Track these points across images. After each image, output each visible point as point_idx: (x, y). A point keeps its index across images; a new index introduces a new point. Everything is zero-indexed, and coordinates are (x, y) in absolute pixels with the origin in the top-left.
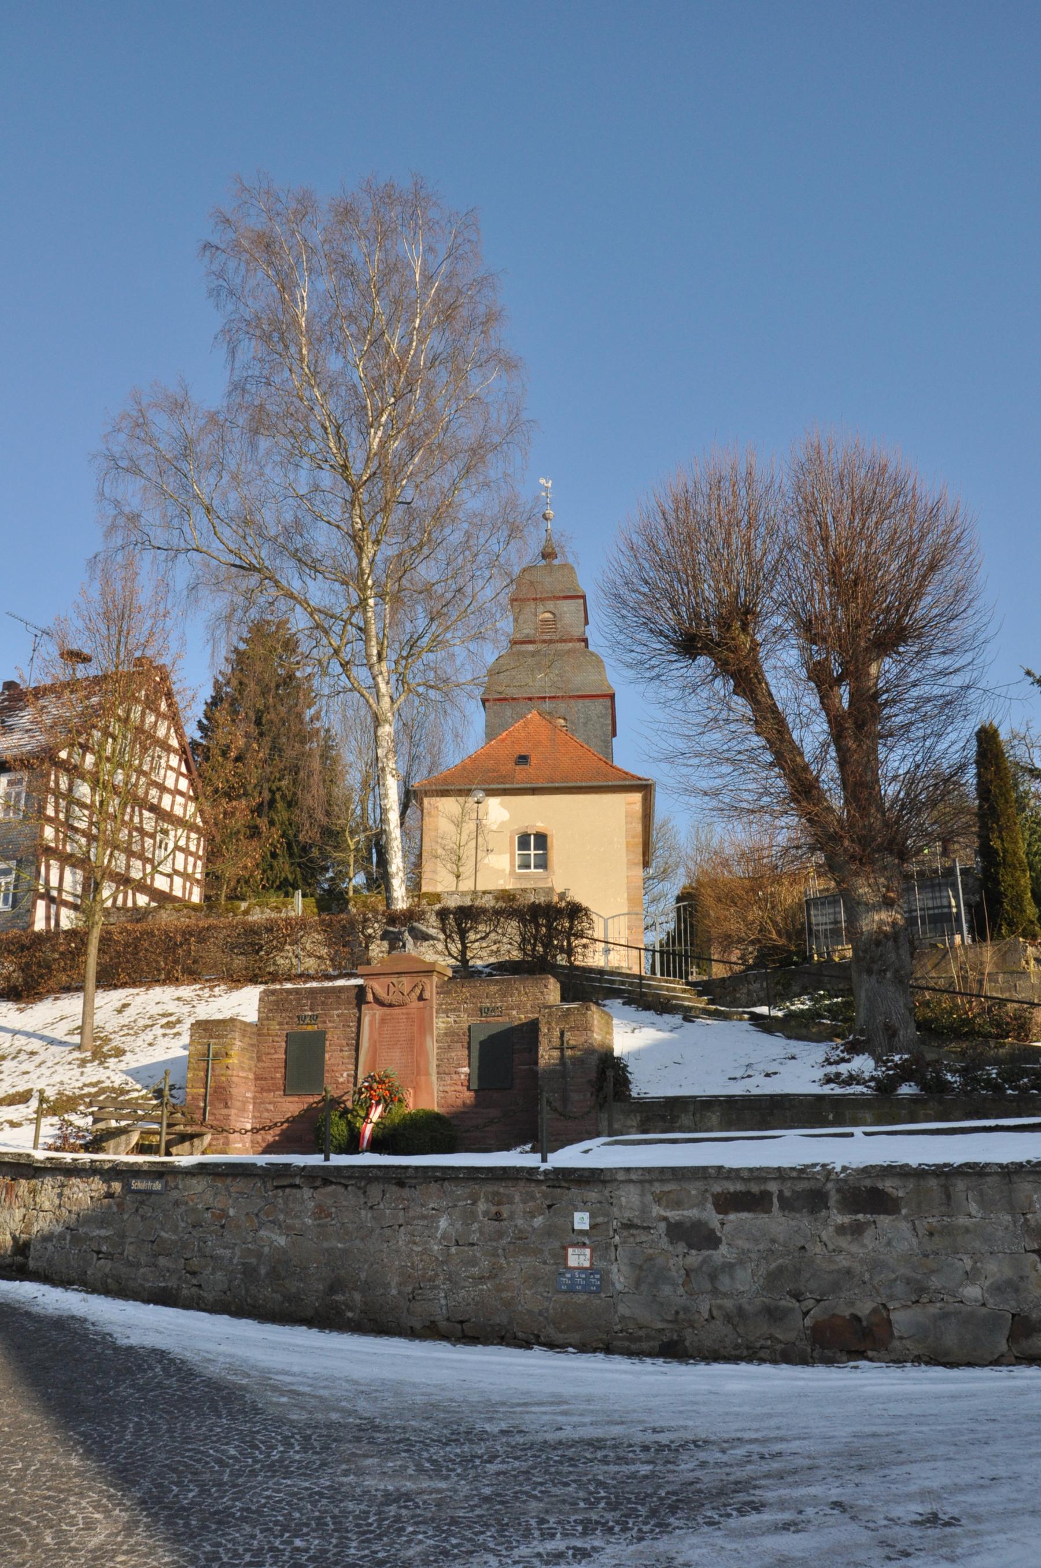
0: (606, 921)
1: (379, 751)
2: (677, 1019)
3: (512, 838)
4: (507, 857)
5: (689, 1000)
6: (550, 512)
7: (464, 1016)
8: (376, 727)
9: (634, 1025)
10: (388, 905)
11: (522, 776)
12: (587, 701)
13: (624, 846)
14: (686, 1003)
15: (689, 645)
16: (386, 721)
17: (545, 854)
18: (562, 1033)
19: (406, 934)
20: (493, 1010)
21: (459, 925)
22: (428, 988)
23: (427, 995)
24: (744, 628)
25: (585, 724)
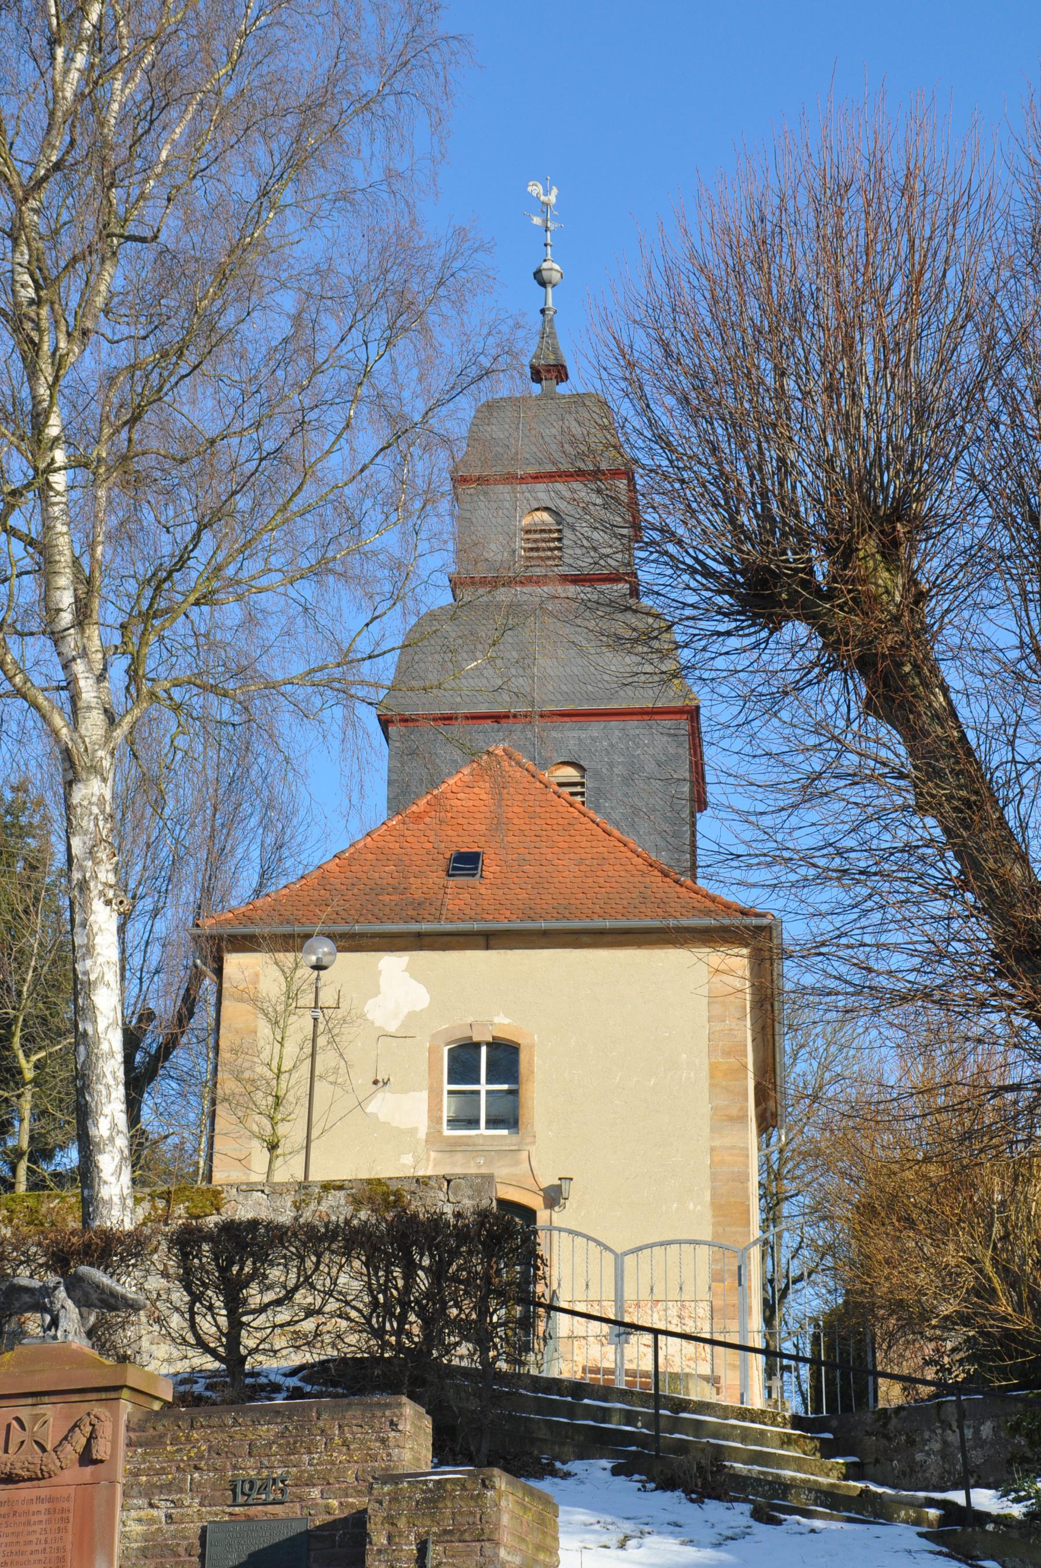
0: (619, 1259)
1: (76, 842)
2: (739, 1515)
3: (433, 1051)
4: (421, 1099)
5: (799, 1465)
6: (553, 268)
7: (192, 1504)
8: (69, 784)
9: (628, 1527)
10: (86, 1218)
11: (462, 902)
12: (633, 725)
13: (705, 1074)
14: (788, 1473)
15: (761, 596)
16: (95, 769)
17: (513, 1093)
18: (422, 1549)
19: (62, 1293)
20: (263, 1489)
21: (224, 1270)
22: (105, 1430)
23: (101, 1450)
24: (890, 550)
25: (628, 780)
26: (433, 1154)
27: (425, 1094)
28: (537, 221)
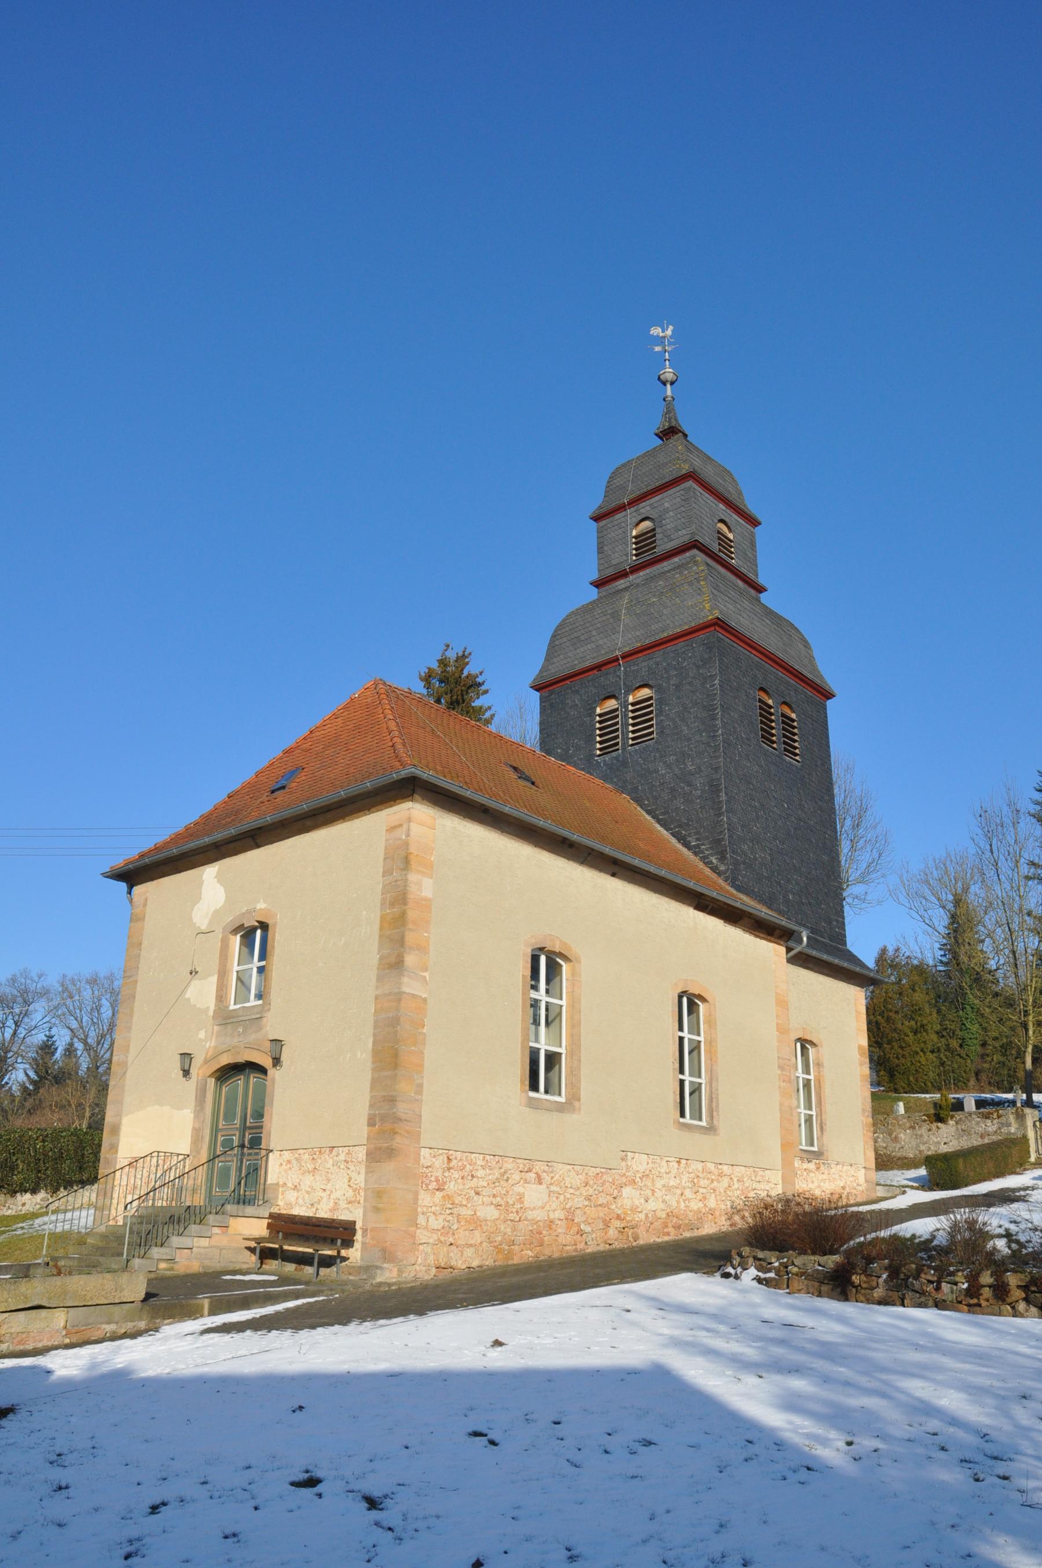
6: (668, 373)
12: (681, 644)
26: (216, 1028)
27: (216, 976)
28: (658, 349)
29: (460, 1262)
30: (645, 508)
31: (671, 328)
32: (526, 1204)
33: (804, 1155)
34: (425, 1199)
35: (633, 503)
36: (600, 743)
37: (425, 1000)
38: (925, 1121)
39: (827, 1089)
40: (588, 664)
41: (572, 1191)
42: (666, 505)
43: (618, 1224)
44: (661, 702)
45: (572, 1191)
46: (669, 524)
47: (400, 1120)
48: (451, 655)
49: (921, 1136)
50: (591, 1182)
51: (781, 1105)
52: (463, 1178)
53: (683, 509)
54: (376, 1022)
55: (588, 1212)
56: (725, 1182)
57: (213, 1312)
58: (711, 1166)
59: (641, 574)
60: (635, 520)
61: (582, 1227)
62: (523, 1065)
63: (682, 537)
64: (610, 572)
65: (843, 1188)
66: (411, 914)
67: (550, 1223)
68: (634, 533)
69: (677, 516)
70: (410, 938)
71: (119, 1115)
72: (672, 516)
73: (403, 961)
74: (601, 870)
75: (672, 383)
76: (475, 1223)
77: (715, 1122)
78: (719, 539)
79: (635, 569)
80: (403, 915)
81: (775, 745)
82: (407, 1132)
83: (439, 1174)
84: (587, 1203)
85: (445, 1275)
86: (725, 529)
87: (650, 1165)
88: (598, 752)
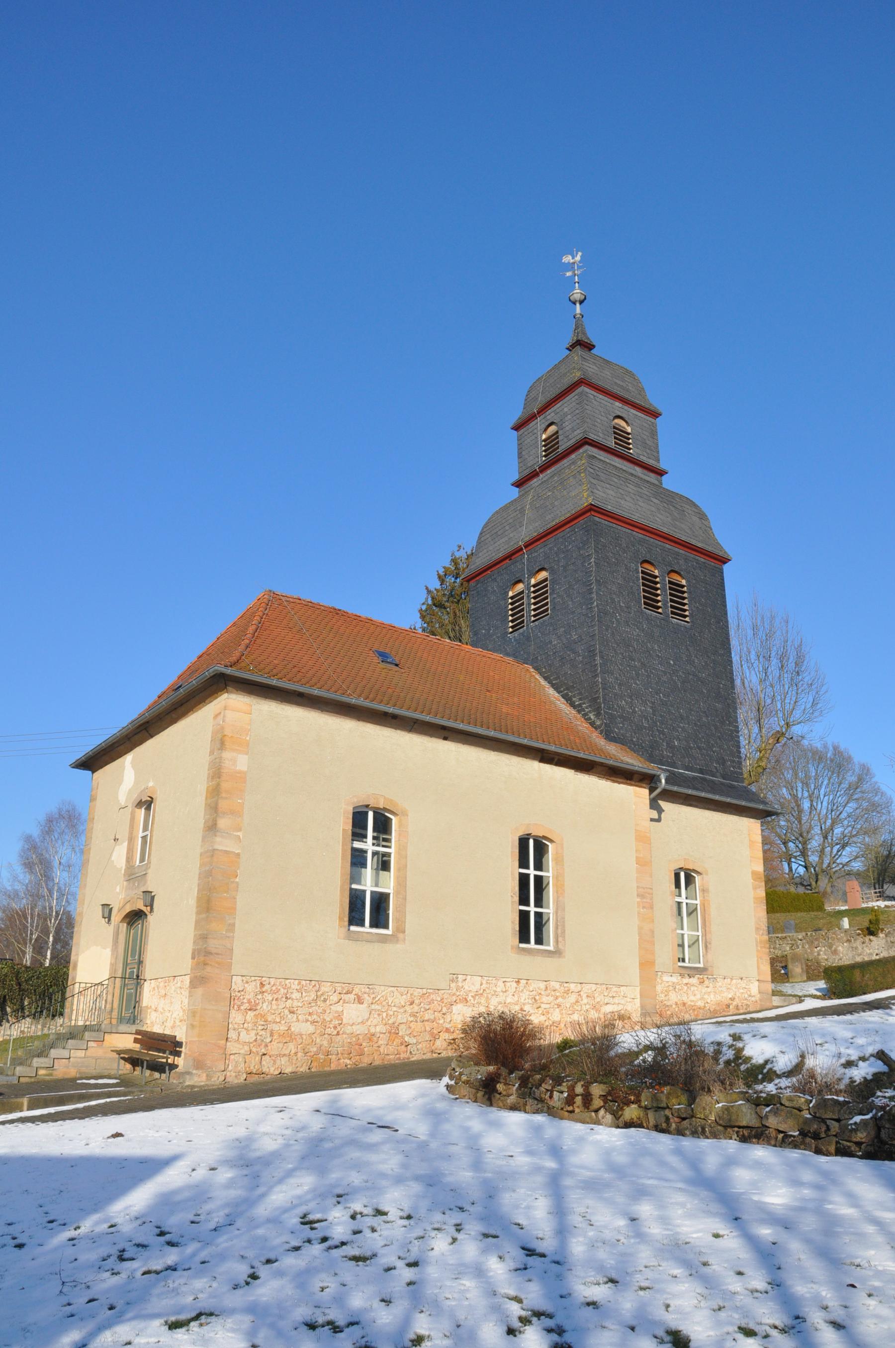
12: (567, 529)
28: (569, 274)
29: (272, 1069)
30: (550, 415)
31: (580, 254)
32: (345, 1021)
33: (683, 971)
34: (236, 1017)
35: (542, 410)
36: (512, 621)
37: (238, 854)
38: (859, 934)
39: (713, 912)
40: (501, 555)
41: (395, 1009)
42: (566, 410)
43: (447, 1036)
44: (554, 582)
45: (395, 1009)
46: (568, 426)
47: (211, 953)
48: (462, 554)
49: (856, 948)
50: (417, 1002)
51: (640, 928)
52: (277, 999)
53: (577, 411)
54: (200, 874)
55: (413, 1027)
56: (573, 998)
57: (30, 1108)
58: (557, 985)
59: (549, 472)
60: (544, 426)
61: (407, 1039)
62: (341, 905)
63: (577, 436)
64: (527, 472)
65: (732, 999)
66: (224, 785)
67: (371, 1037)
68: (544, 437)
69: (596, 415)
70: (223, 805)
71: (77, 955)
72: (582, 417)
73: (216, 824)
74: (431, 736)
75: (581, 302)
76: (289, 1036)
77: (560, 946)
78: (615, 433)
79: (544, 468)
80: (218, 785)
81: (660, 610)
82: (219, 963)
83: (251, 996)
84: (412, 1019)
85: (254, 1079)
86: (623, 423)
87: (484, 986)
88: (511, 630)
